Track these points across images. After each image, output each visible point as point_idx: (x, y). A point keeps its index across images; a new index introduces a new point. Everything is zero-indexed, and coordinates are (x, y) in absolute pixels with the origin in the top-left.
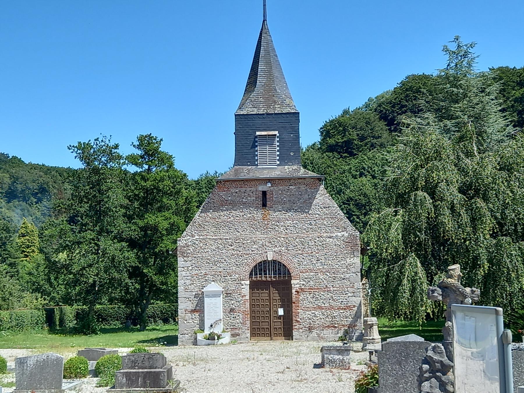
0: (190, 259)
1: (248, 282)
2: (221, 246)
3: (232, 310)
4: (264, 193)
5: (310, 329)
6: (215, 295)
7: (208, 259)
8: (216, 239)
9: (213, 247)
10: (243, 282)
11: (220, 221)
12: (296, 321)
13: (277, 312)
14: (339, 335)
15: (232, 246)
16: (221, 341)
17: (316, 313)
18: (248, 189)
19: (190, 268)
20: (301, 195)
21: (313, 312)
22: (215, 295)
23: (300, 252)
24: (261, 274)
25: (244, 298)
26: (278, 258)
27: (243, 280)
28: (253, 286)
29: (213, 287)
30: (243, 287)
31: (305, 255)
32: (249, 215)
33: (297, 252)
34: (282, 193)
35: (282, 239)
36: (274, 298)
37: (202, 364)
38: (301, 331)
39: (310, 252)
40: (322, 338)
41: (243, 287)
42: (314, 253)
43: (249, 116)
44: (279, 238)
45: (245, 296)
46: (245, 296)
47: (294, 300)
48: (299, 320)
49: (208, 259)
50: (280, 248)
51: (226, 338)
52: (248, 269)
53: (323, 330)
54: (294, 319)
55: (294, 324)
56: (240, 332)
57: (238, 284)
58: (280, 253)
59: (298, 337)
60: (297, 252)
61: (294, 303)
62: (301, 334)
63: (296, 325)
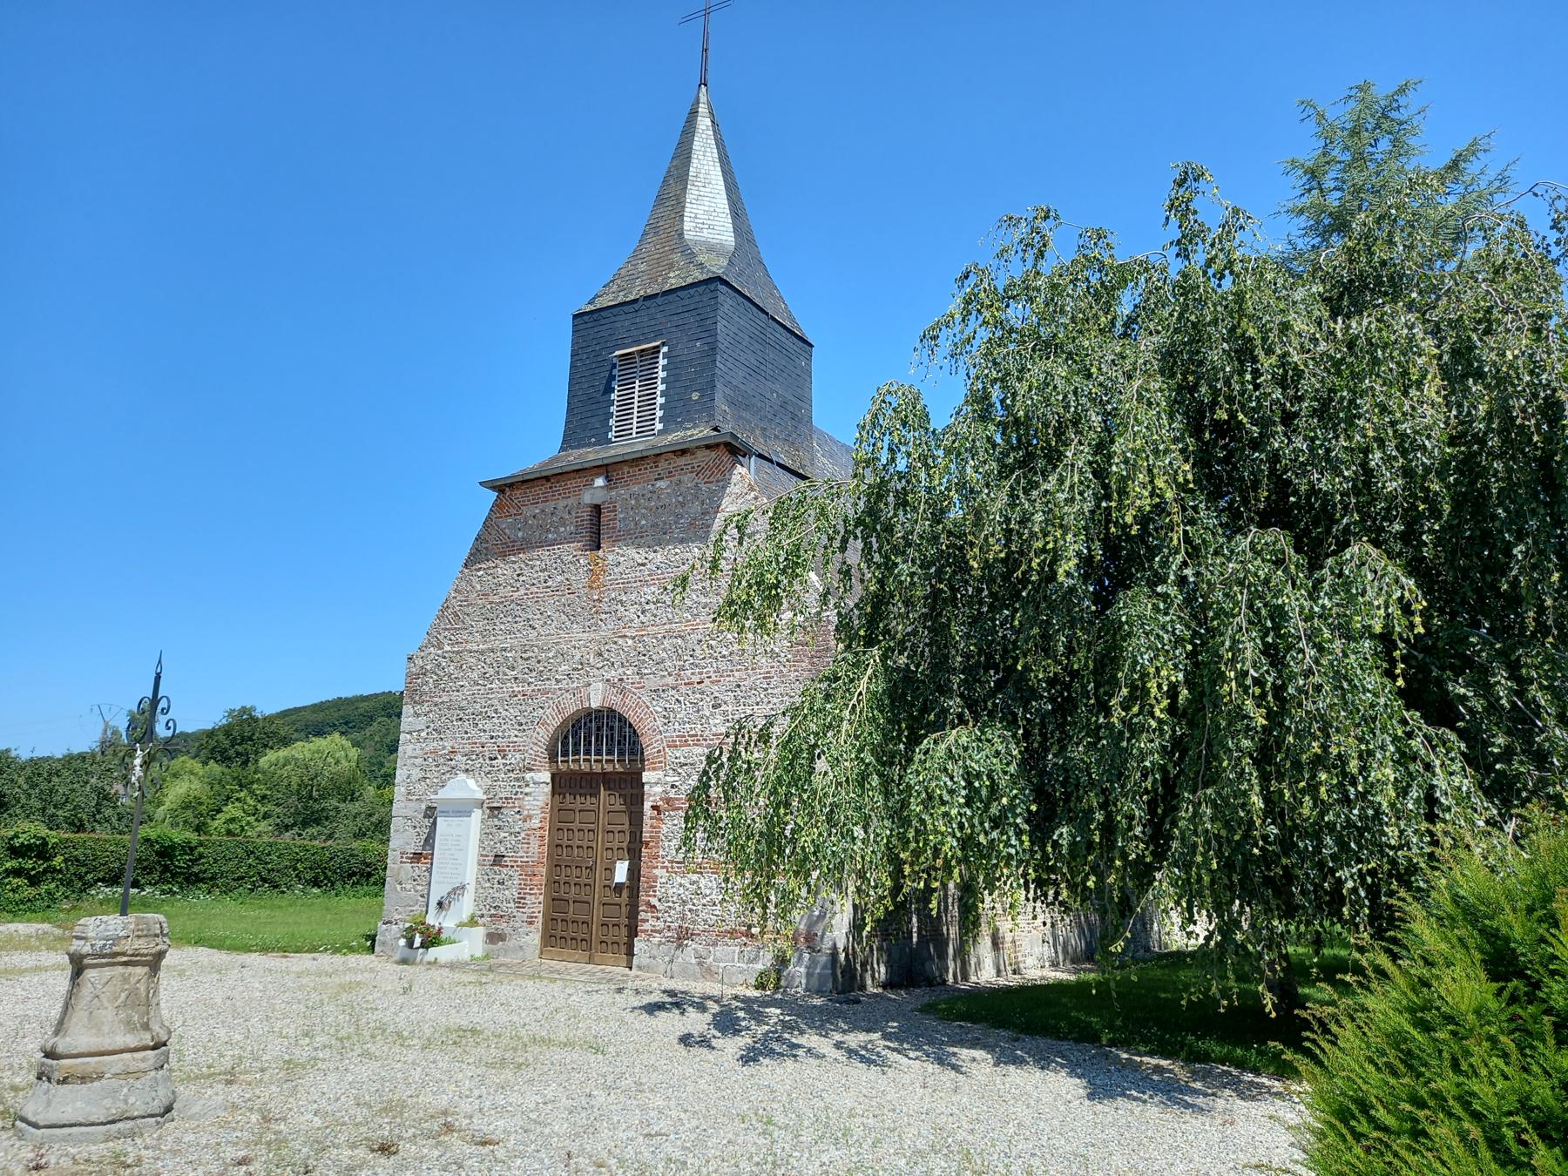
0: (425, 708)
1: (546, 776)
2: (491, 671)
3: (498, 859)
4: (597, 509)
5: (683, 936)
6: (461, 809)
7: (461, 709)
8: (482, 653)
9: (475, 675)
10: (528, 776)
11: (497, 599)
12: (648, 904)
13: (610, 870)
14: (760, 967)
15: (513, 669)
16: (434, 952)
17: (703, 883)
18: (561, 504)
19: (423, 734)
20: (683, 504)
21: (695, 877)
22: (461, 809)
23: (670, 680)
24: (576, 752)
25: (527, 825)
26: (615, 701)
27: (531, 770)
28: (562, 784)
29: (467, 787)
30: (527, 790)
31: (683, 689)
32: (559, 578)
33: (665, 681)
34: (638, 506)
35: (630, 642)
36: (610, 827)
37: (656, 997)
38: (655, 941)
39: (696, 679)
40: (709, 970)
41: (527, 790)
42: (707, 681)
43: (603, 314)
44: (620, 641)
45: (530, 817)
46: (530, 817)
47: (646, 836)
48: (654, 901)
49: (461, 709)
50: (621, 671)
51: (471, 944)
52: (543, 735)
53: (715, 944)
54: (643, 898)
55: (642, 915)
56: (508, 930)
57: (517, 780)
58: (619, 686)
59: (645, 961)
60: (665, 681)
61: (647, 843)
62: (654, 952)
63: (648, 922)
